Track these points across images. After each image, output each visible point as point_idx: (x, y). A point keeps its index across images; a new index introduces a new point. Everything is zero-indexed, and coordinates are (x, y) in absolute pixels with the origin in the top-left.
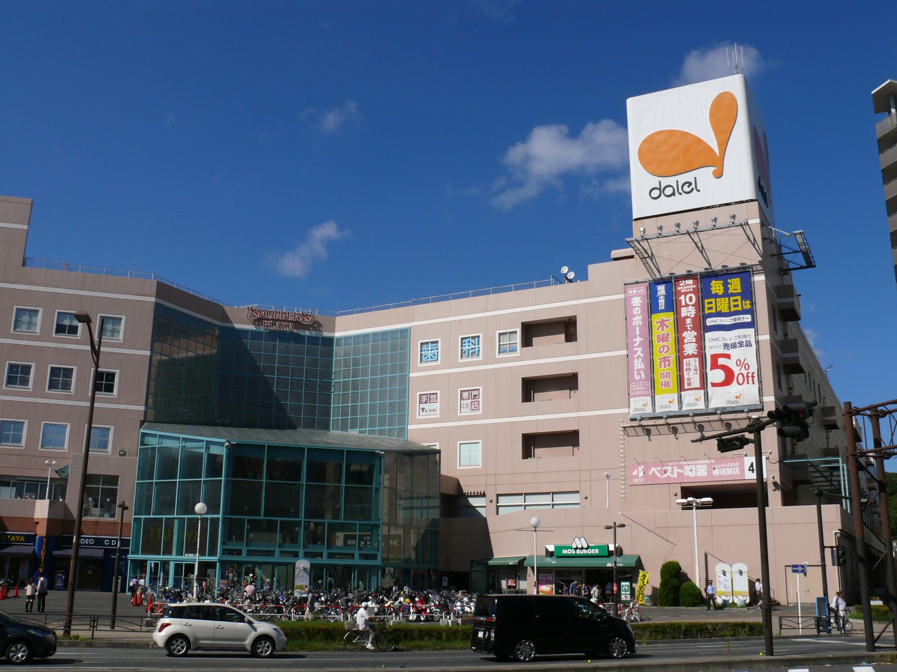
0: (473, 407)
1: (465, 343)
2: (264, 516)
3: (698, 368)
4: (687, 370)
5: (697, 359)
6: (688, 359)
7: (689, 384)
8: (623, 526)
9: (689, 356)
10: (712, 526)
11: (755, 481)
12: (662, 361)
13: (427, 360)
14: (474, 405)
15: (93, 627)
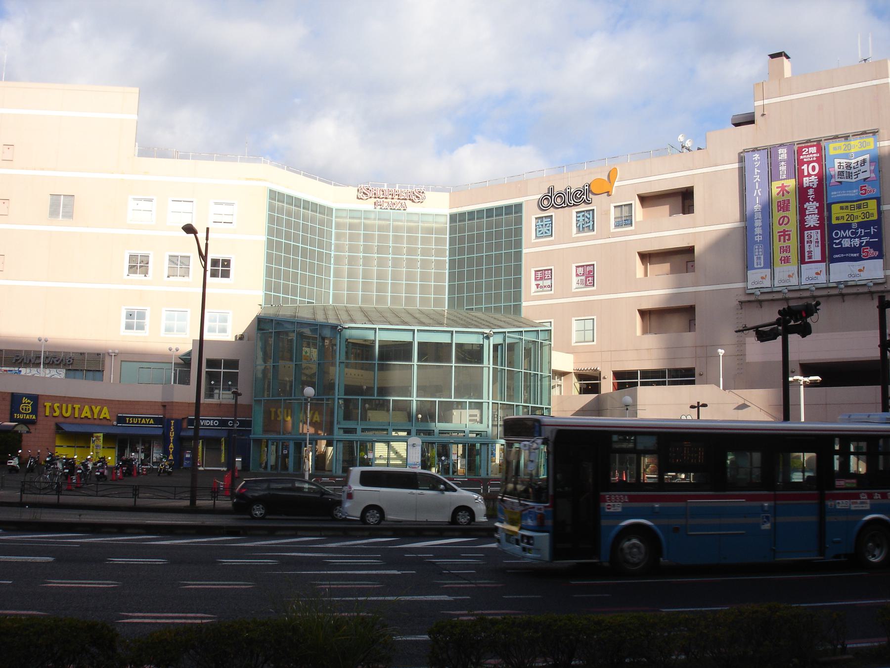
0: (588, 282)
1: (579, 217)
2: (377, 396)
3: (819, 240)
4: (807, 243)
5: (819, 231)
6: (809, 232)
7: (810, 257)
8: (705, 405)
9: (810, 228)
10: (826, 404)
11: (879, 359)
12: (781, 235)
13: (542, 235)
14: (589, 280)
15: (135, 496)
